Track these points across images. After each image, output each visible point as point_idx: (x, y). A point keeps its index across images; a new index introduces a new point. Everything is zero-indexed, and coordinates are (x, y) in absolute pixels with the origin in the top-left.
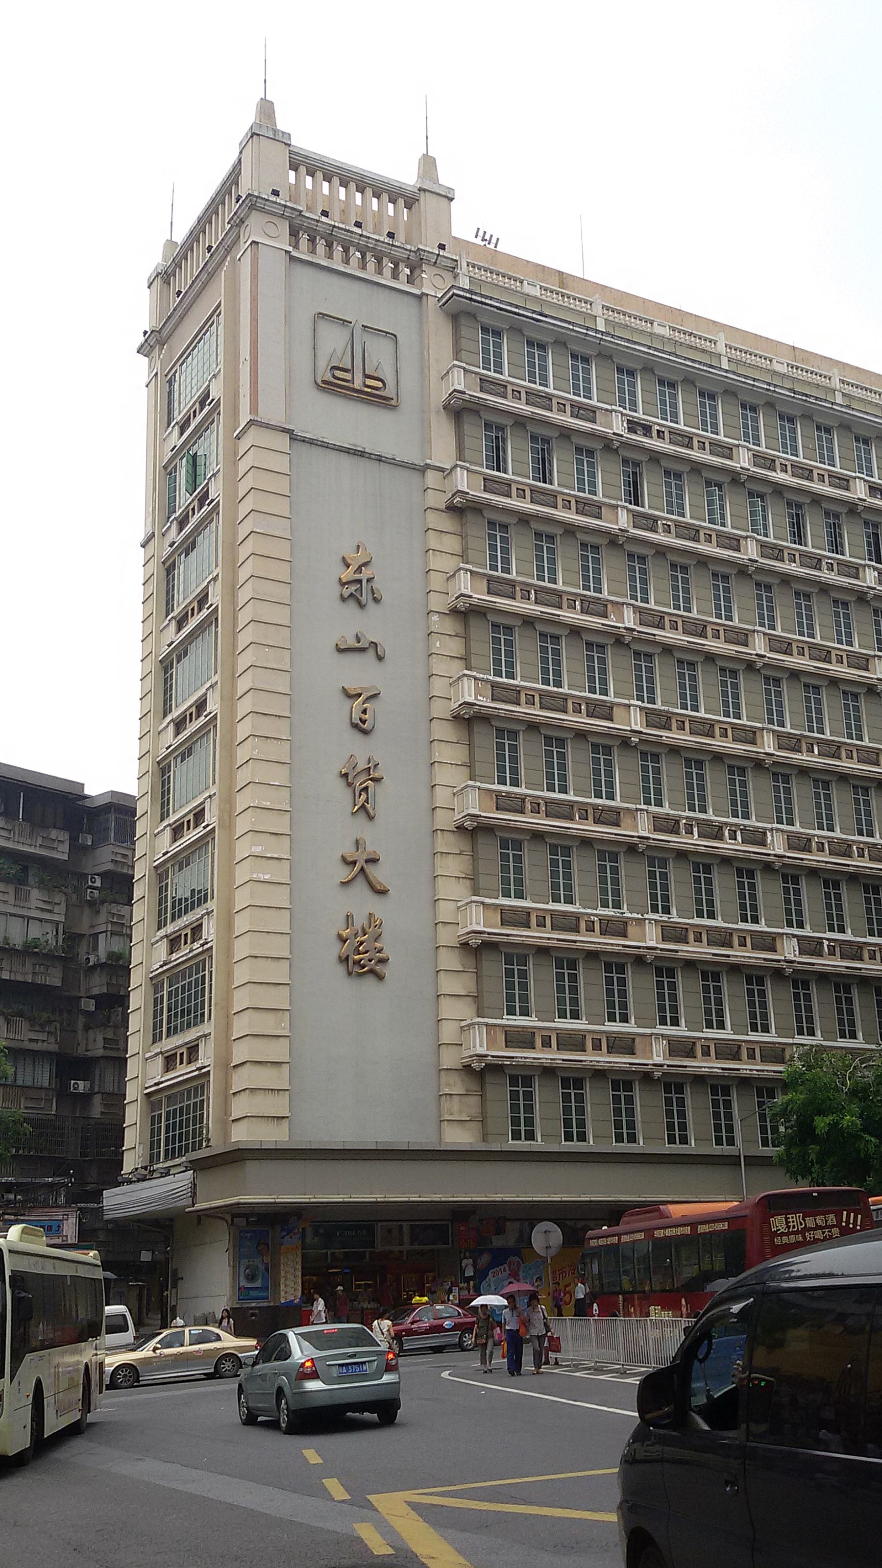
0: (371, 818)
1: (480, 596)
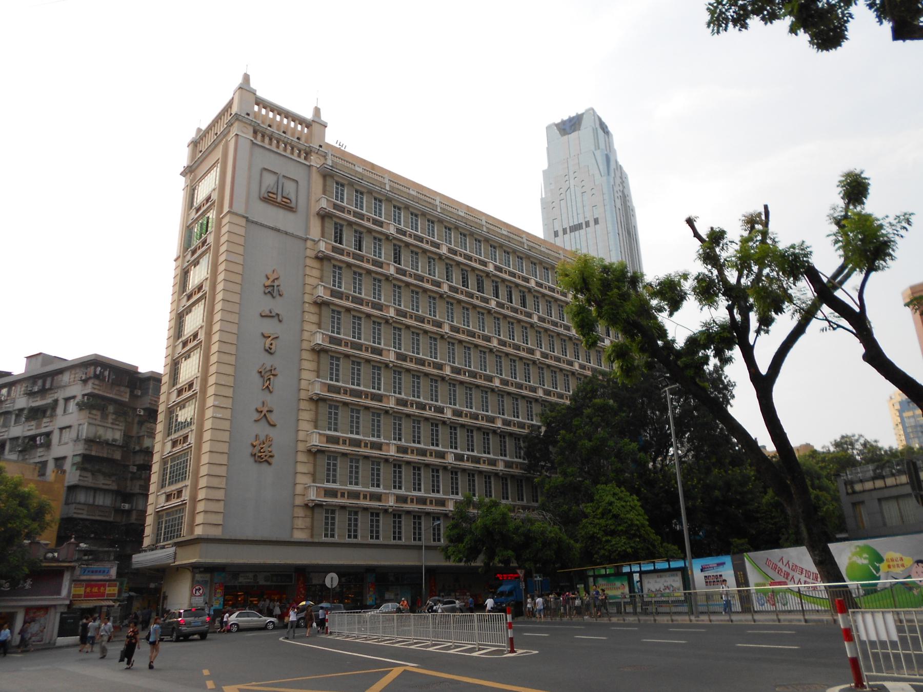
0: (271, 392)
1: (327, 297)
